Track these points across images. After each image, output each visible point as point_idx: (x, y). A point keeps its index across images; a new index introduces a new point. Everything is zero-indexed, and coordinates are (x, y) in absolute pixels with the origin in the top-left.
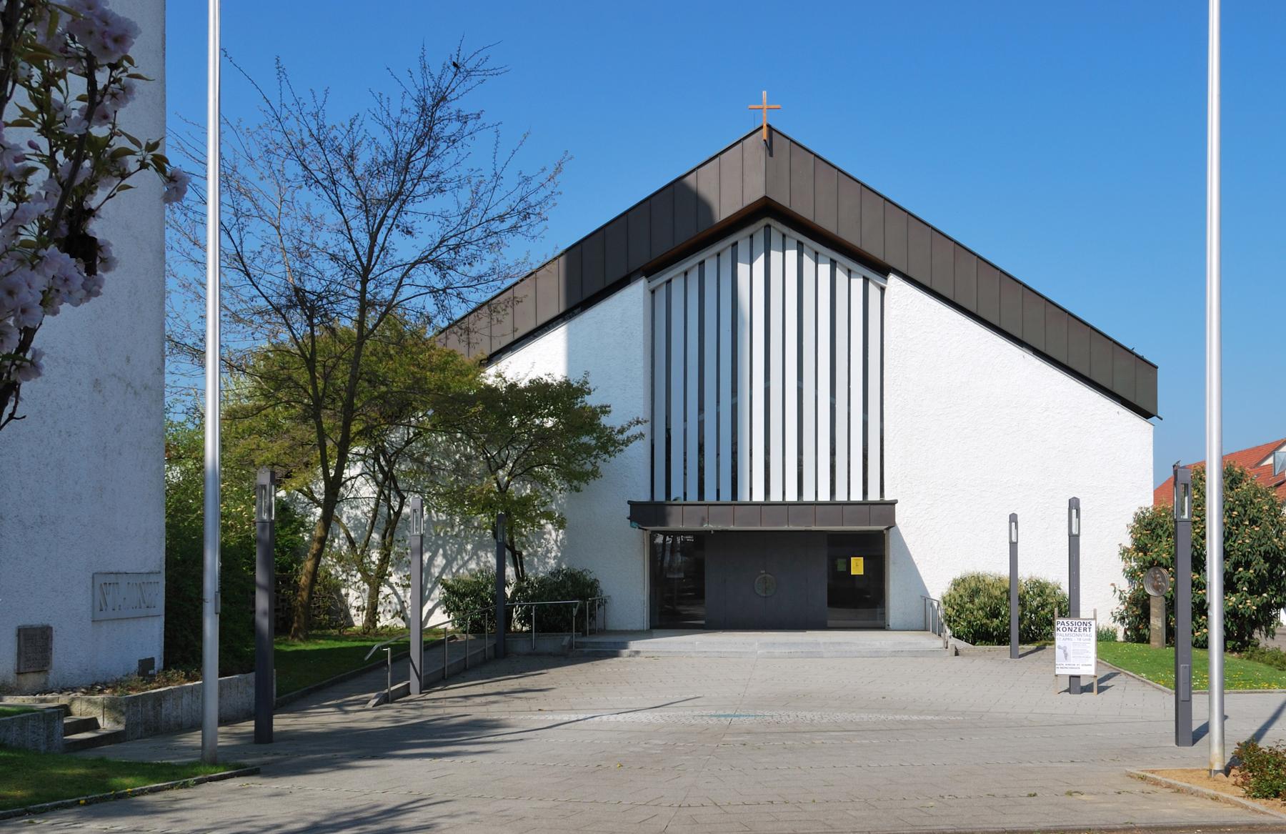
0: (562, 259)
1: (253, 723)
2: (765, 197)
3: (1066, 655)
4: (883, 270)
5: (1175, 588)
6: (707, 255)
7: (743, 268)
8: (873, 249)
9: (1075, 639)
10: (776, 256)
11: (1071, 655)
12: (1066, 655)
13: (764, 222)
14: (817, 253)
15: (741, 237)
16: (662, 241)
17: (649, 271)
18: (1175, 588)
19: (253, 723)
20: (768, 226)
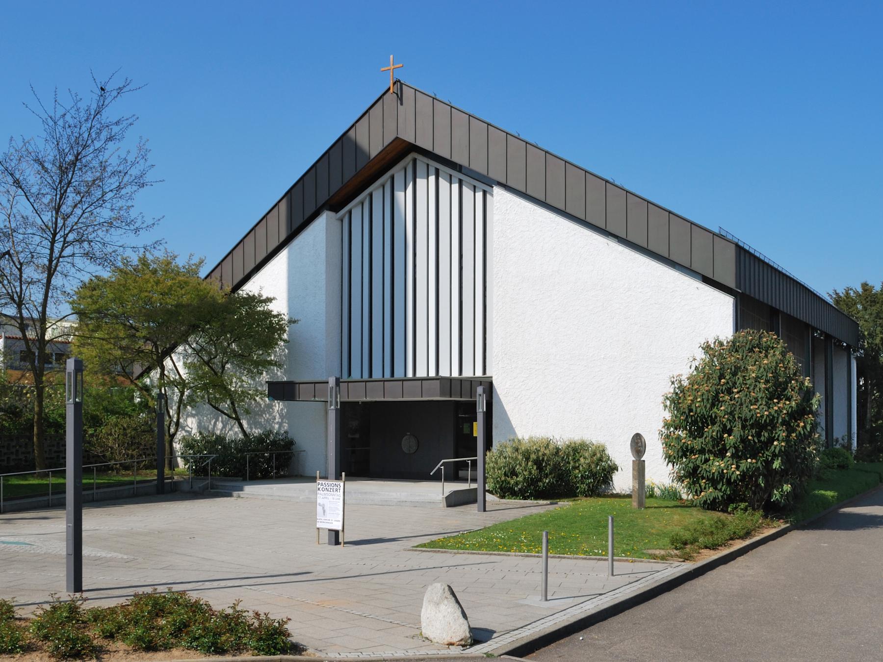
0: (284, 200)
1: (156, 471)
2: (397, 138)
3: (324, 511)
4: (485, 182)
5: (485, 455)
6: (375, 189)
7: (399, 195)
8: (478, 166)
9: (330, 497)
10: (421, 182)
11: (327, 511)
12: (324, 511)
13: (410, 157)
14: (475, 187)
15: (397, 171)
16: (344, 183)
17: (336, 204)
18: (485, 455)
19: (156, 471)
20: (415, 161)
